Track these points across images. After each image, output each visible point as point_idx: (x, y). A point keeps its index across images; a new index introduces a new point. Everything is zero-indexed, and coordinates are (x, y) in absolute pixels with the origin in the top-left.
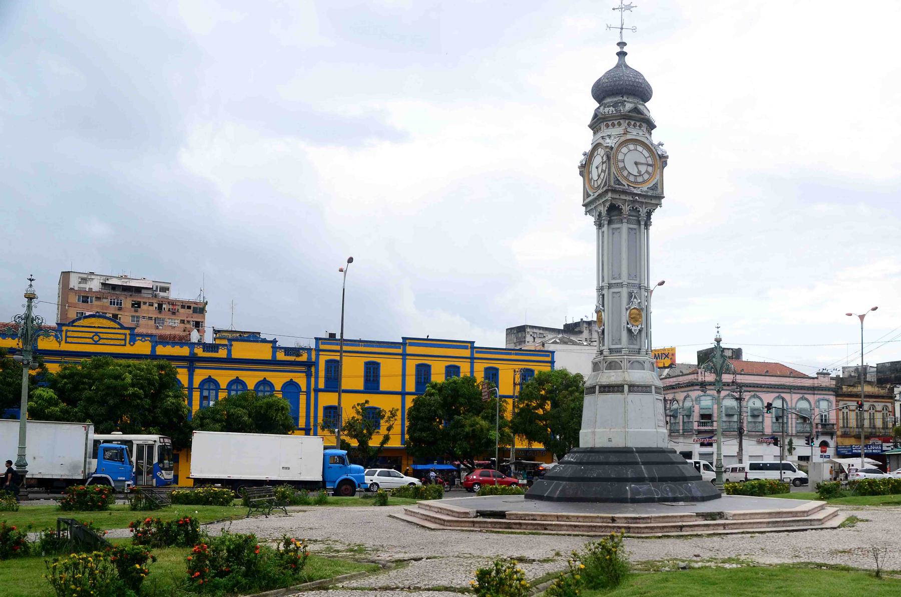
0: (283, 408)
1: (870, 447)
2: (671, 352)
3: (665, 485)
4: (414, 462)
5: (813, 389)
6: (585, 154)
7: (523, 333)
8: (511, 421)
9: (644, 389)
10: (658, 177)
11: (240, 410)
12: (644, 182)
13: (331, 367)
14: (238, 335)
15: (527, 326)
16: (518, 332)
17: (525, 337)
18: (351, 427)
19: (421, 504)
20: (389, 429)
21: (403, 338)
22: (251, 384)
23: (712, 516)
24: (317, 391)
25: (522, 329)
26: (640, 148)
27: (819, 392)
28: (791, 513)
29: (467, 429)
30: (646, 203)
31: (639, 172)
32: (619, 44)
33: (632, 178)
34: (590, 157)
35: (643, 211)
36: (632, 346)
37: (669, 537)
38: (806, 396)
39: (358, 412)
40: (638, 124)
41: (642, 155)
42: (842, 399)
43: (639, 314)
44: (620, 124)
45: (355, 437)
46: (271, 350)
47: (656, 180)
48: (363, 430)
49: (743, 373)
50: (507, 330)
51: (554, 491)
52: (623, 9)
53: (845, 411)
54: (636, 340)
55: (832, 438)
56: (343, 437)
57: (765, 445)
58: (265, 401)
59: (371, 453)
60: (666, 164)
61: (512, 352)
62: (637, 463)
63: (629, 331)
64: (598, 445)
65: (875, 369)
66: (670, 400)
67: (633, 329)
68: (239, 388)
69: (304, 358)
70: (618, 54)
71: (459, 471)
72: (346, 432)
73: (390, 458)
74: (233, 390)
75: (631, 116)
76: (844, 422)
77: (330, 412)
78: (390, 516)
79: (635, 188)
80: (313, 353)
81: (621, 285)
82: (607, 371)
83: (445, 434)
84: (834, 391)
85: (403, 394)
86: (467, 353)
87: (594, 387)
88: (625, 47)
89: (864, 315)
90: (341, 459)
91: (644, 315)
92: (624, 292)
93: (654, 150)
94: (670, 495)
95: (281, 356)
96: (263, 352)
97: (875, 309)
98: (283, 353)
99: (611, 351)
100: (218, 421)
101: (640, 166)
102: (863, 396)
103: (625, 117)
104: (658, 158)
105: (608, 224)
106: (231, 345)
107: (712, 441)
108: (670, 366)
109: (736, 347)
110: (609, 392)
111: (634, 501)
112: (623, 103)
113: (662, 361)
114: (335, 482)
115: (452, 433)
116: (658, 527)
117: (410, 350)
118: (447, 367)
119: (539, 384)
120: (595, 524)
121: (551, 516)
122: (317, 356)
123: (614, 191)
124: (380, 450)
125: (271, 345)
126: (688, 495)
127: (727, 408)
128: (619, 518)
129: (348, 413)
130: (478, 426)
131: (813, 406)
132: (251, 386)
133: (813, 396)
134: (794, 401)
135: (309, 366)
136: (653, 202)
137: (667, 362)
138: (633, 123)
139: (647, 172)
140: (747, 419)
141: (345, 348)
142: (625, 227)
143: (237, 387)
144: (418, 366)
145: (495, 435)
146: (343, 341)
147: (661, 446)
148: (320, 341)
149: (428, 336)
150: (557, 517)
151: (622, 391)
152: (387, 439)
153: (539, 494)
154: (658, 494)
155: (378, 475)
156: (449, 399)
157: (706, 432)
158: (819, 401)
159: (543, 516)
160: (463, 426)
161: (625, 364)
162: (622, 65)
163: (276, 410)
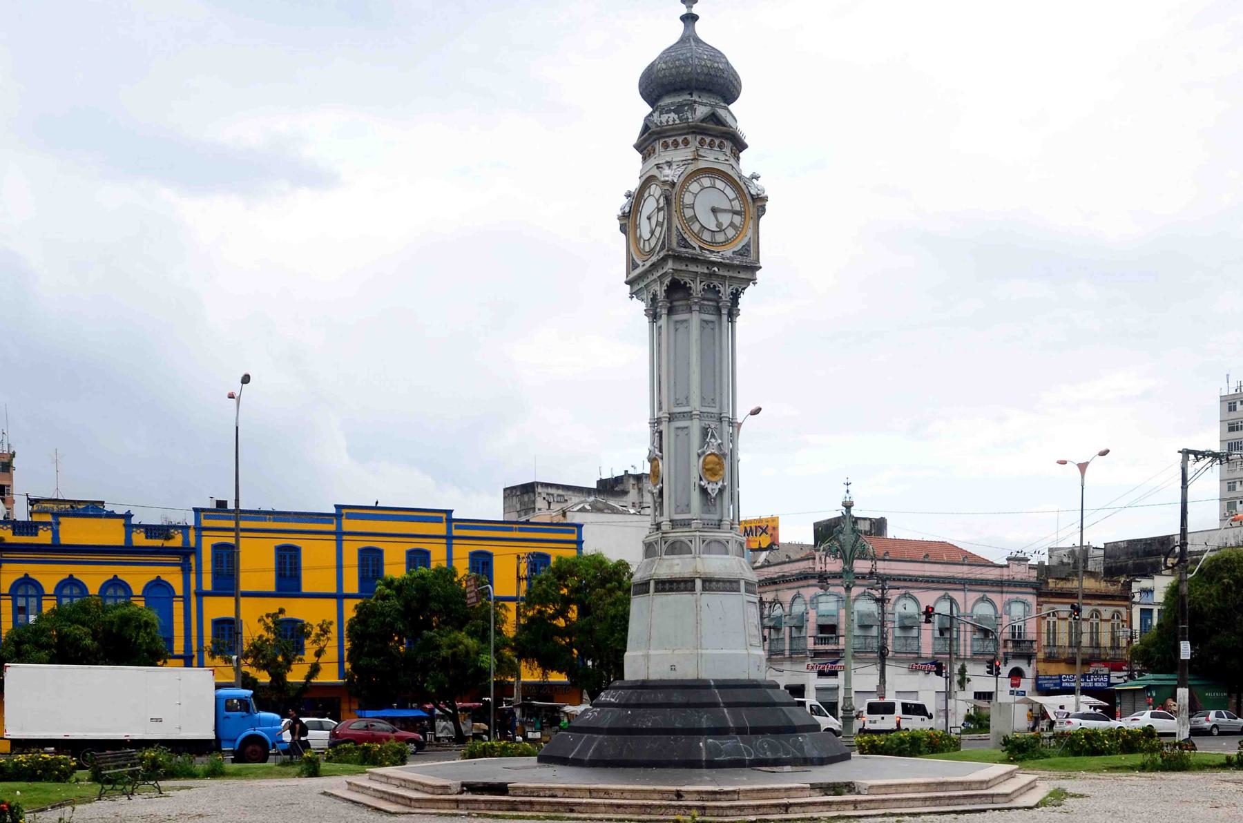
0: (147, 624)
1: (1089, 679)
3: (760, 738)
5: (1000, 585)
7: (532, 495)
8: (515, 639)
9: (728, 585)
10: (750, 233)
11: (78, 629)
12: (727, 242)
14: (68, 506)
15: (538, 483)
16: (522, 494)
17: (534, 502)
18: (258, 652)
19: (372, 773)
20: (318, 654)
21: (337, 507)
23: (835, 788)
24: (201, 594)
26: (720, 184)
27: (1011, 589)
29: (445, 652)
30: (731, 277)
31: (719, 225)
33: (706, 236)
34: (637, 199)
35: (726, 291)
38: (989, 595)
39: (268, 629)
40: (717, 142)
41: (723, 195)
42: (1047, 600)
43: (719, 464)
44: (686, 143)
45: (265, 667)
46: (123, 529)
47: (746, 239)
48: (277, 657)
49: (887, 558)
50: (505, 490)
53: (1052, 619)
55: (1029, 664)
56: (245, 669)
57: (921, 674)
58: (118, 612)
59: (292, 694)
60: (764, 211)
61: (514, 526)
62: (716, 705)
63: (704, 491)
67: (710, 487)
68: (74, 592)
69: (177, 541)
71: (432, 719)
72: (250, 661)
75: (705, 129)
77: (223, 629)
79: (712, 252)
80: (192, 534)
81: (689, 416)
82: (667, 557)
84: (1034, 588)
85: (340, 597)
86: (441, 529)
89: (1086, 464)
92: (695, 426)
93: (744, 187)
94: (769, 755)
95: (139, 539)
96: (112, 535)
98: (143, 535)
99: (674, 523)
103: (697, 130)
104: (750, 200)
106: (58, 523)
107: (836, 669)
108: (770, 548)
110: (671, 590)
111: (712, 765)
112: (691, 106)
113: (758, 538)
114: (235, 740)
115: (420, 659)
117: (348, 525)
118: (410, 553)
120: (650, 802)
121: (580, 790)
122: (199, 538)
123: (677, 258)
124: (306, 687)
125: (123, 521)
126: (799, 755)
127: (861, 615)
128: (688, 792)
129: (253, 629)
130: (461, 647)
131: (999, 612)
132: (94, 588)
134: (971, 605)
135: (185, 556)
136: (742, 275)
137: (765, 541)
138: (708, 140)
139: (732, 224)
141: (243, 524)
142: (695, 319)
144: (363, 552)
146: (239, 514)
148: (202, 514)
149: (377, 503)
150: (590, 791)
151: (693, 590)
152: (315, 669)
153: (560, 753)
154: (749, 754)
158: (1009, 603)
159: (567, 789)
160: (438, 647)
161: (696, 546)
162: (690, 38)
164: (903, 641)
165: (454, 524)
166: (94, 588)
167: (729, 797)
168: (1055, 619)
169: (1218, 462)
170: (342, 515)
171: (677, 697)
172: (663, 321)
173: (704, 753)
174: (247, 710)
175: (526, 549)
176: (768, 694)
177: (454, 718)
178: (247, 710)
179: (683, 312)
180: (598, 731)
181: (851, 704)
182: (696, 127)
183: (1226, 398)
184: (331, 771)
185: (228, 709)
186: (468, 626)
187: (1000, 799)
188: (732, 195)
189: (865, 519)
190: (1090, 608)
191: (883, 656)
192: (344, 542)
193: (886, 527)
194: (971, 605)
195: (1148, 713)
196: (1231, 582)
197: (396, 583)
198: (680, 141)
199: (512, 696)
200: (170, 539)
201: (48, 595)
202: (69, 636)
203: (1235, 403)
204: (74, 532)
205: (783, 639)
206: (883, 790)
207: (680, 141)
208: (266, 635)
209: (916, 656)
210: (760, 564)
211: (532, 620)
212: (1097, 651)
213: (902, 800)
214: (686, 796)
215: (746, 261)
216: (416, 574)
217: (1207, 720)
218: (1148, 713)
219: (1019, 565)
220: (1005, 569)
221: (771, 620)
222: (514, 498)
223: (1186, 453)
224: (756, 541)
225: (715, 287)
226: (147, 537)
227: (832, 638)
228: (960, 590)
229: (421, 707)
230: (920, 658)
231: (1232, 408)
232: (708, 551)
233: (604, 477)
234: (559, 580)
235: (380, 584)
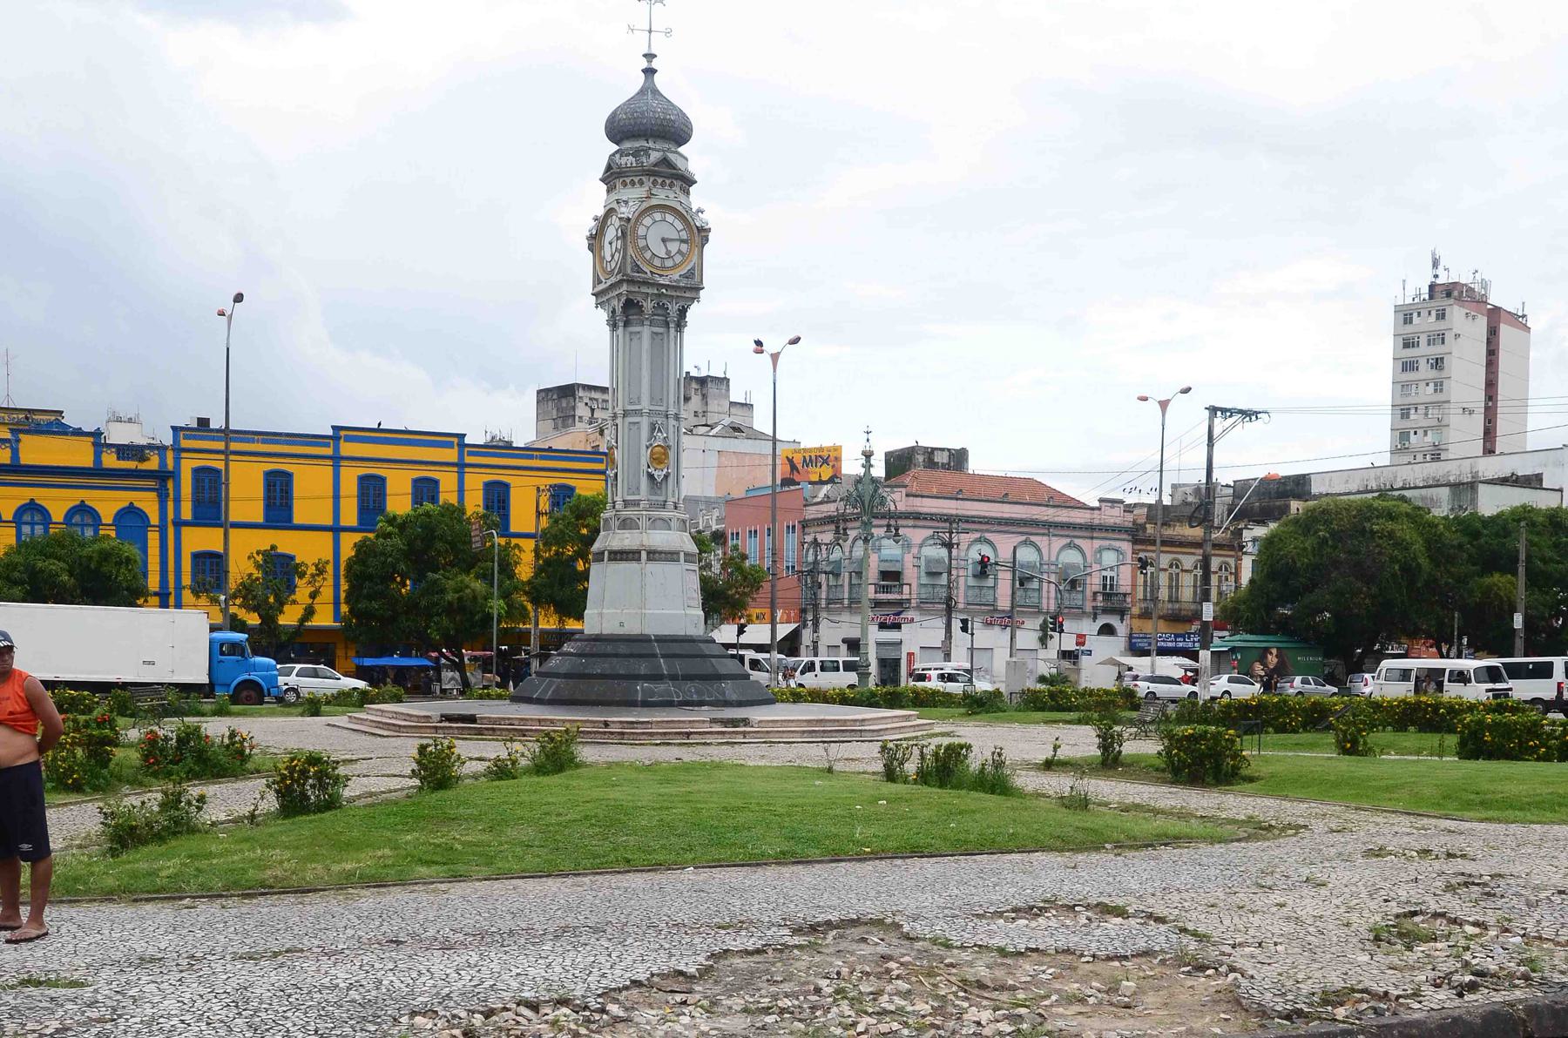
0: (128, 560)
1: (1189, 638)
2: (833, 454)
3: (689, 684)
4: (357, 652)
5: (1091, 529)
6: (596, 219)
7: (571, 399)
8: (529, 582)
9: (670, 556)
10: (695, 259)
11: (54, 564)
12: (675, 266)
13: (203, 480)
14: (21, 416)
15: (579, 385)
16: (560, 398)
17: (574, 408)
18: (247, 592)
19: (370, 709)
20: (313, 596)
21: (333, 427)
22: (58, 512)
23: (734, 722)
24: (179, 524)
25: (568, 391)
26: (670, 218)
27: (1103, 535)
28: (838, 721)
29: (450, 597)
31: (668, 252)
32: (645, 56)
33: (657, 262)
34: (602, 223)
35: (673, 308)
36: (654, 498)
37: (669, 744)
38: (1077, 541)
39: (258, 566)
40: (668, 182)
41: (672, 227)
42: (1144, 547)
43: (664, 454)
44: (641, 183)
45: (255, 609)
46: (92, 450)
47: (692, 264)
48: (268, 598)
49: (960, 496)
50: (539, 392)
51: (545, 691)
54: (660, 488)
55: (1122, 620)
56: (233, 610)
57: (997, 629)
58: (96, 547)
59: (284, 638)
60: (707, 240)
61: (535, 453)
62: (654, 656)
63: (651, 477)
64: (605, 632)
65: (1231, 491)
66: (826, 544)
67: (656, 474)
68: (36, 518)
69: (153, 464)
70: (646, 71)
71: (438, 669)
72: (238, 601)
73: (312, 645)
74: (26, 523)
75: (656, 171)
76: (1145, 590)
77: (204, 563)
78: (329, 725)
79: (661, 276)
80: (170, 456)
81: (639, 413)
83: (412, 606)
85: (336, 530)
86: (451, 455)
87: (603, 553)
88: (654, 60)
89: (1168, 401)
90: (235, 648)
91: (672, 454)
92: (645, 422)
93: (690, 219)
94: (695, 697)
95: (110, 461)
96: (80, 455)
97: (1186, 391)
99: (626, 503)
100: (16, 583)
101: (668, 244)
102: (1158, 542)
103: (650, 173)
104: (696, 231)
105: (625, 326)
106: (18, 441)
107: (900, 621)
108: (831, 480)
109: (956, 445)
111: (646, 704)
112: (646, 151)
113: (818, 470)
114: (229, 685)
115: (423, 603)
116: (657, 733)
117: (347, 449)
118: (416, 482)
119: (578, 518)
121: (532, 719)
122: (177, 460)
123: (631, 281)
124: (300, 630)
125: (92, 439)
126: (721, 698)
127: (929, 561)
128: (613, 722)
129: (241, 567)
130: (468, 591)
131: (1089, 560)
132: (58, 514)
133: (1089, 541)
134: (1059, 553)
135: (162, 479)
136: (687, 295)
137: (826, 473)
138: (660, 181)
139: (679, 252)
140: (964, 580)
141: (234, 446)
142: (646, 331)
143: (33, 518)
145: (497, 605)
146: (227, 433)
147: (692, 634)
148: (182, 433)
149: (379, 424)
150: (539, 720)
151: (639, 559)
152: (309, 612)
153: (526, 695)
154: (678, 696)
155: (297, 675)
156: (419, 542)
157: (889, 603)
158: (1100, 550)
159: (522, 719)
160: (443, 591)
161: (643, 523)
162: (649, 90)
163: (116, 563)
164: (977, 591)
165: (466, 449)
167: (644, 726)
168: (1177, 571)
169: (1248, 419)
170: (340, 438)
171: (623, 649)
173: (640, 695)
174: (242, 655)
175: (546, 481)
176: (701, 649)
177: (459, 667)
178: (242, 655)
179: (637, 324)
180: (557, 675)
181: (867, 659)
182: (648, 170)
183: (1401, 308)
184: (330, 712)
185: (222, 653)
186: (476, 569)
187: (867, 734)
189: (942, 450)
190: (1219, 560)
191: (949, 610)
192: (342, 468)
193: (967, 459)
194: (1059, 553)
195: (1226, 677)
196: (1328, 535)
197: (399, 521)
199: (529, 645)
200: (145, 461)
201: (4, 522)
202: (44, 571)
203: (1411, 314)
204: (36, 451)
205: (842, 586)
206: (771, 724)
208: (257, 574)
209: (992, 608)
210: (819, 500)
211: (548, 562)
212: (1177, 606)
213: (783, 732)
214: (612, 725)
216: (420, 511)
217: (1292, 687)
218: (1226, 677)
219: (1112, 507)
220: (1096, 512)
221: (829, 563)
222: (550, 403)
223: (1213, 410)
224: (815, 473)
226: (118, 459)
227: (895, 586)
228: (1043, 534)
229: (424, 655)
230: (996, 610)
231: (1408, 320)
234: (577, 520)
235: (382, 521)
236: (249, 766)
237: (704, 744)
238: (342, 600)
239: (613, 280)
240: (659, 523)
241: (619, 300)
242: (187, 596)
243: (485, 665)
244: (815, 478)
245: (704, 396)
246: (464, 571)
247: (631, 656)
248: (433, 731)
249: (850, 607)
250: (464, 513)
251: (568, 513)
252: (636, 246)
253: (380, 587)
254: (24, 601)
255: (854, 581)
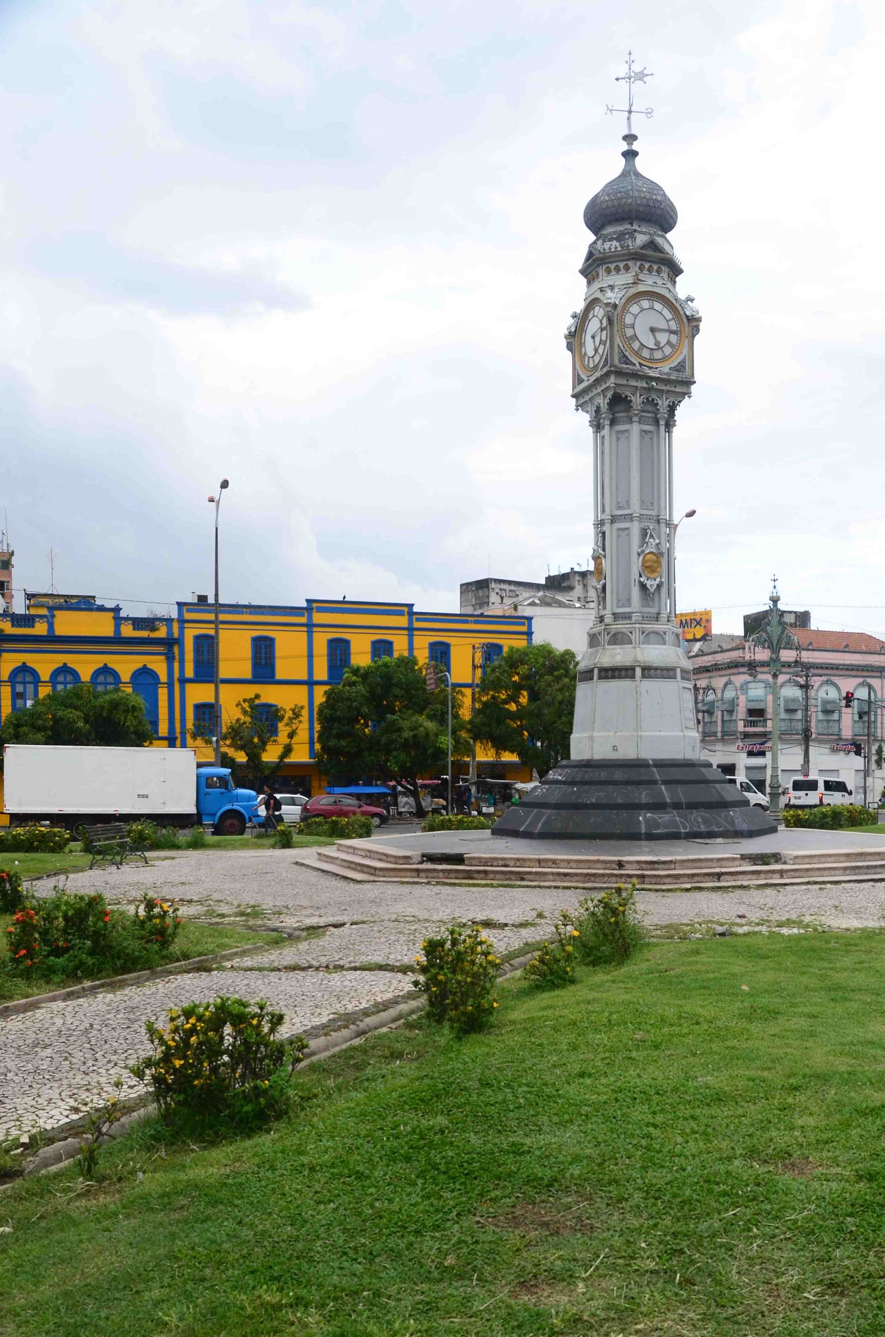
0: (134, 708)
2: (704, 617)
6: (574, 316)
7: (486, 590)
8: (470, 722)
9: (666, 672)
10: (685, 351)
11: (71, 713)
12: (665, 359)
15: (491, 579)
17: (488, 597)
18: (235, 734)
19: (340, 845)
20: (291, 736)
21: (308, 601)
24: (183, 681)
25: (483, 585)
26: (658, 306)
29: (406, 734)
30: (668, 391)
31: (657, 343)
32: (625, 138)
33: (646, 353)
34: (582, 319)
35: (663, 404)
37: (700, 889)
39: (245, 712)
40: (655, 267)
41: (661, 316)
43: (656, 562)
44: (627, 268)
46: (112, 621)
47: (682, 356)
48: (253, 738)
49: (811, 648)
51: (534, 823)
52: (632, 80)
54: (653, 600)
56: (224, 749)
58: (107, 697)
59: (267, 772)
60: (698, 331)
61: (470, 619)
62: (655, 782)
63: (643, 587)
64: (597, 757)
67: (648, 583)
68: (68, 679)
69: (162, 633)
71: (395, 795)
72: (228, 742)
75: (644, 255)
77: (204, 713)
80: (176, 626)
81: (629, 518)
82: (609, 647)
83: (373, 744)
85: (311, 683)
86: (403, 621)
92: (635, 528)
93: (679, 308)
94: (703, 828)
95: (127, 631)
98: (131, 627)
100: (40, 729)
101: (658, 335)
103: (636, 256)
106: (53, 616)
108: (704, 638)
110: (613, 677)
111: (650, 837)
112: (632, 234)
113: (692, 630)
114: (214, 815)
115: (384, 740)
117: (319, 618)
121: (529, 860)
122: (182, 630)
123: (619, 373)
124: (279, 766)
125: (112, 614)
126: (731, 828)
127: (787, 701)
128: (628, 862)
130: (421, 729)
136: (678, 389)
137: (699, 632)
139: (669, 343)
141: (222, 617)
142: (635, 429)
143: (65, 679)
144: (197, 638)
145: (447, 741)
146: (219, 607)
150: (539, 861)
151: (633, 677)
152: (288, 750)
154: (685, 828)
159: (518, 860)
160: (400, 730)
162: (630, 172)
163: (125, 711)
165: (414, 617)
166: (86, 675)
170: (313, 609)
171: (619, 775)
172: (606, 431)
176: (703, 773)
177: (414, 794)
181: (778, 781)
184: (302, 843)
188: (669, 316)
189: (790, 612)
192: (315, 634)
197: (362, 671)
198: (622, 267)
199: (468, 774)
205: (716, 722)
206: (807, 860)
207: (622, 267)
208: (243, 718)
209: (836, 737)
211: (485, 705)
214: (627, 866)
215: (681, 376)
216: (380, 663)
225: (653, 400)
229: (384, 784)
232: (647, 642)
233: (552, 574)
236: (175, 948)
237: (742, 887)
238: (316, 740)
239: (598, 374)
240: (652, 636)
241: (605, 396)
242: (189, 740)
243: (437, 792)
244: (690, 637)
245: (585, 586)
246: (417, 712)
247: (627, 783)
248: (415, 874)
249: (723, 739)
250: (416, 664)
251: (503, 663)
252: (623, 335)
253: (346, 727)
254: (46, 743)
255: (726, 718)
